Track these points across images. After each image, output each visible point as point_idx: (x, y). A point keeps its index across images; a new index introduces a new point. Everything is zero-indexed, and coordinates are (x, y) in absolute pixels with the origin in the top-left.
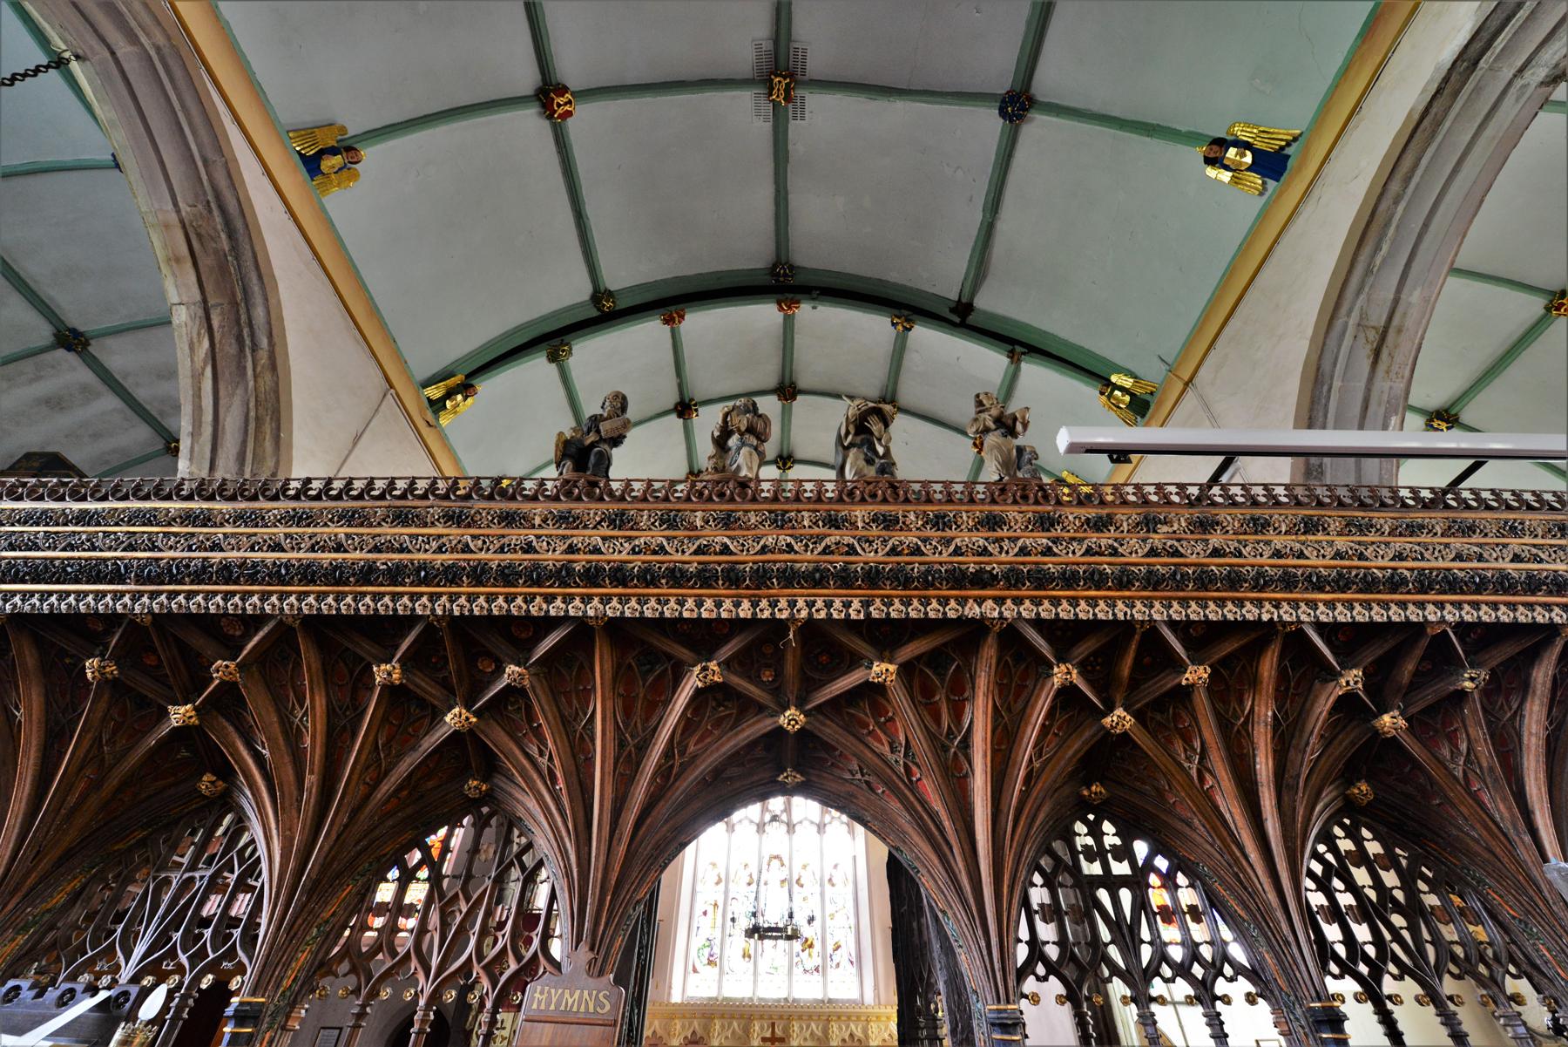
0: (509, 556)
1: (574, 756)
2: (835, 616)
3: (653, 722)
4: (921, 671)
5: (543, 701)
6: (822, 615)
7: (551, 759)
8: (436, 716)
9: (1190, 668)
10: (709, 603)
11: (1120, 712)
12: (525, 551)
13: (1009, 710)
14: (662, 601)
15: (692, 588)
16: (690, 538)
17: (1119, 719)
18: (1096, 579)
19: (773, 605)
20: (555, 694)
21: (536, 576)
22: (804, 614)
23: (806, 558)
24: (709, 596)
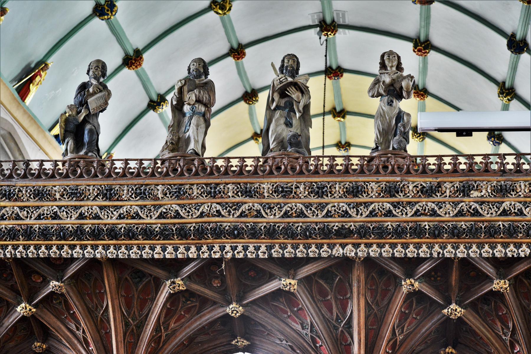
0: (43, 221)
1: (99, 332)
2: (249, 256)
3: (145, 312)
4: (316, 281)
5: (75, 299)
6: (241, 256)
7: (84, 332)
8: (10, 308)
9: (495, 282)
10: (170, 249)
11: (453, 306)
12: (54, 219)
13: (377, 304)
14: (141, 248)
15: (159, 240)
16: (155, 206)
17: (455, 310)
18: (418, 231)
19: (210, 249)
20: (81, 295)
21: (63, 234)
22: (229, 255)
23: (229, 220)
24: (170, 244)
